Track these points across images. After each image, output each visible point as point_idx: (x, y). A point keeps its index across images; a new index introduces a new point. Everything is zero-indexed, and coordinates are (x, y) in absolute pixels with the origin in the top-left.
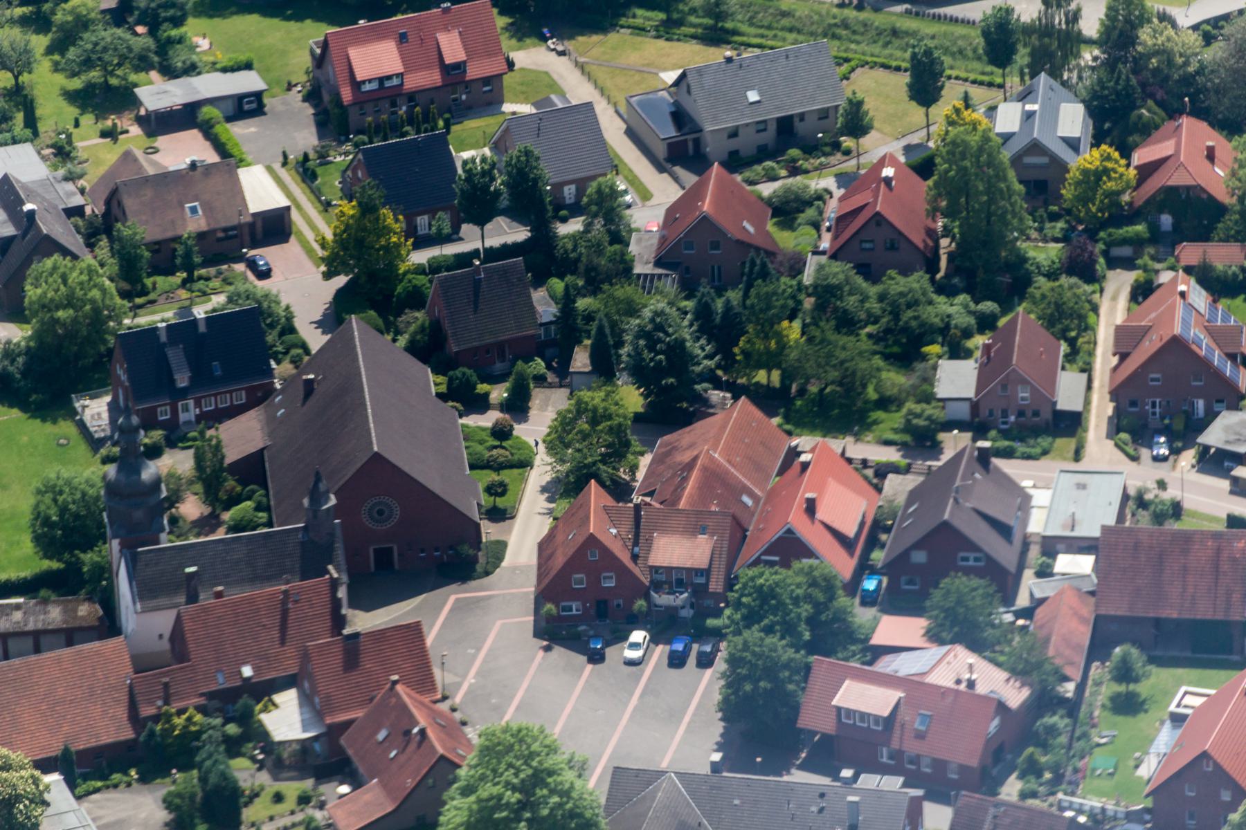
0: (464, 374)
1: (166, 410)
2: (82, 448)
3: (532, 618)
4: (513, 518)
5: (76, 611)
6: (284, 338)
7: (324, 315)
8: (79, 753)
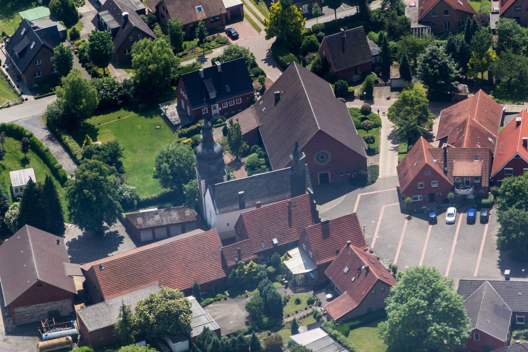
0: (342, 83)
1: (206, 110)
2: (168, 130)
3: (399, 203)
4: (378, 153)
5: (184, 213)
6: (252, 69)
7: (267, 56)
8: (201, 285)
